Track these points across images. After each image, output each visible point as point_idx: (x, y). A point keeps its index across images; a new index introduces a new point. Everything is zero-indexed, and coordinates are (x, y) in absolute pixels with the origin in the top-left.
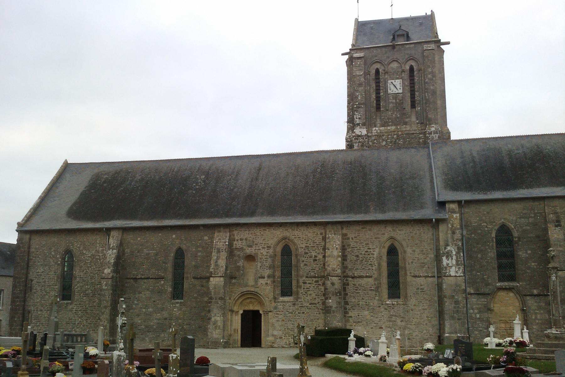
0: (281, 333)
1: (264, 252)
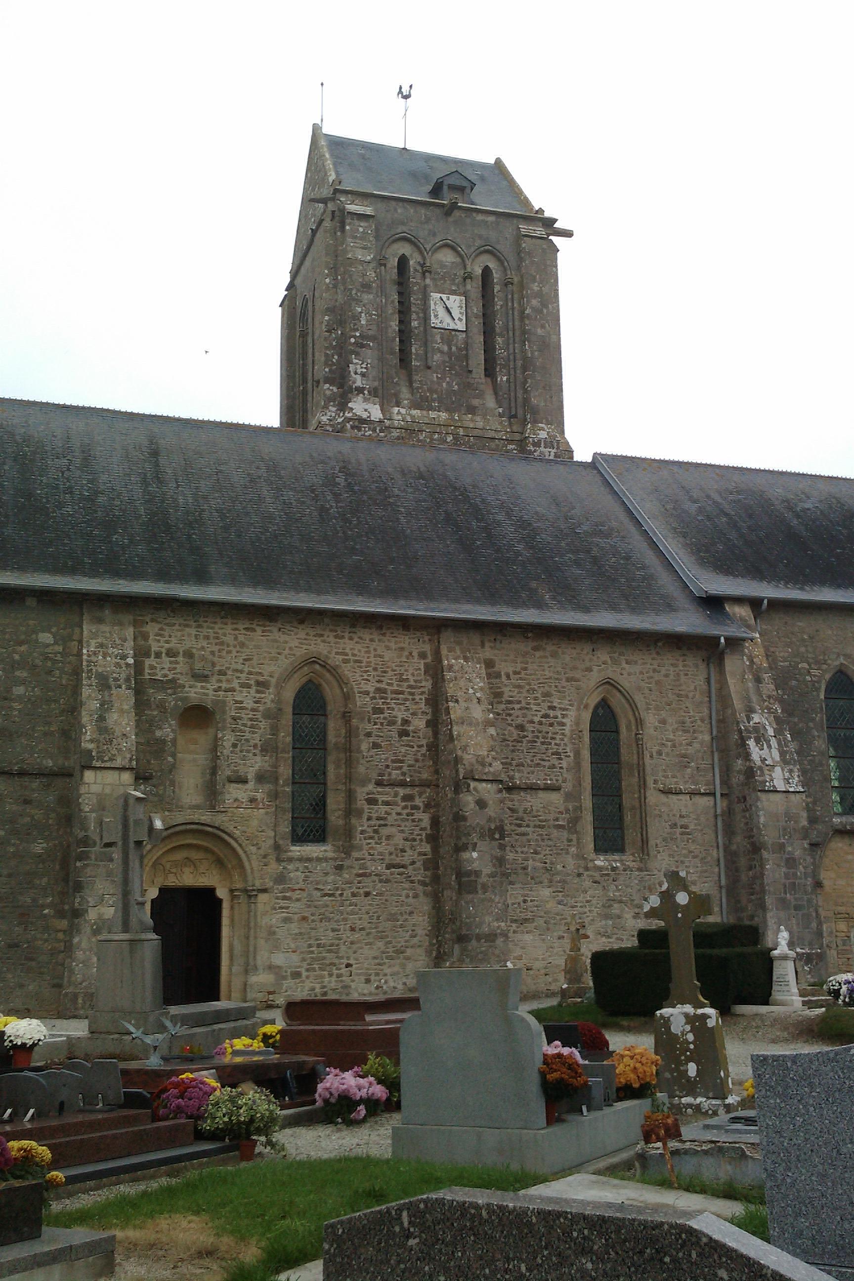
0: (295, 958)
1: (247, 698)
